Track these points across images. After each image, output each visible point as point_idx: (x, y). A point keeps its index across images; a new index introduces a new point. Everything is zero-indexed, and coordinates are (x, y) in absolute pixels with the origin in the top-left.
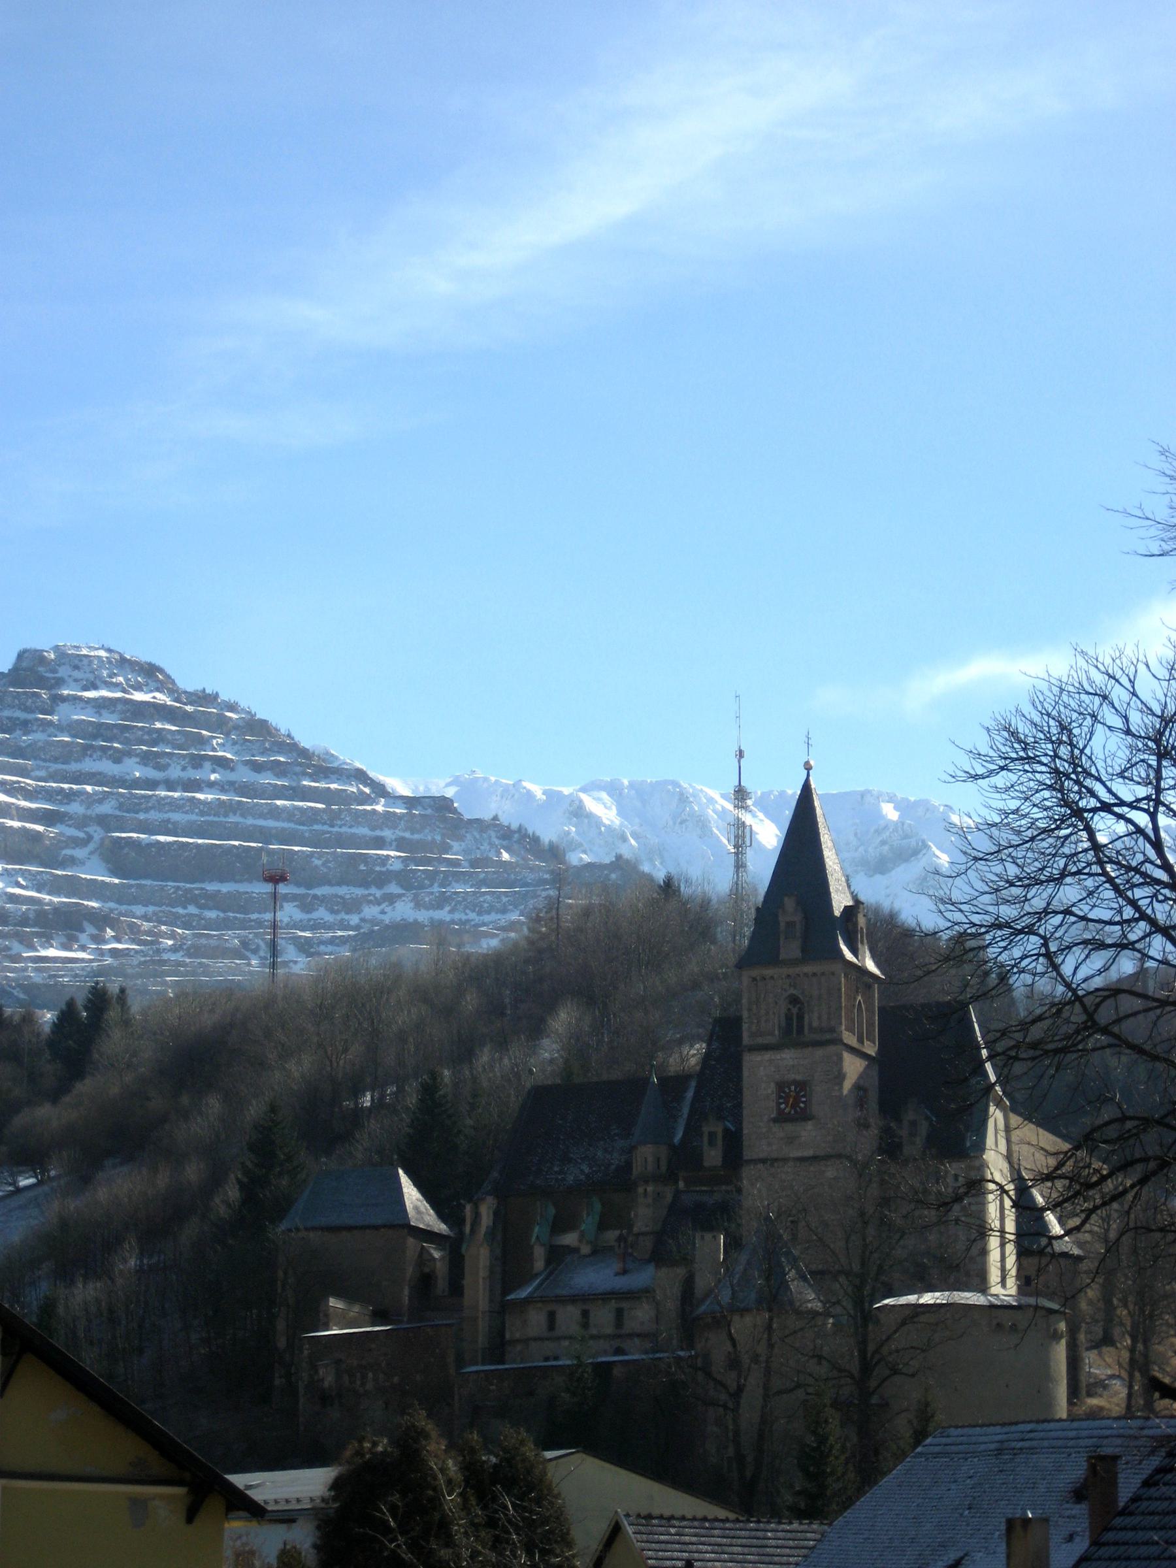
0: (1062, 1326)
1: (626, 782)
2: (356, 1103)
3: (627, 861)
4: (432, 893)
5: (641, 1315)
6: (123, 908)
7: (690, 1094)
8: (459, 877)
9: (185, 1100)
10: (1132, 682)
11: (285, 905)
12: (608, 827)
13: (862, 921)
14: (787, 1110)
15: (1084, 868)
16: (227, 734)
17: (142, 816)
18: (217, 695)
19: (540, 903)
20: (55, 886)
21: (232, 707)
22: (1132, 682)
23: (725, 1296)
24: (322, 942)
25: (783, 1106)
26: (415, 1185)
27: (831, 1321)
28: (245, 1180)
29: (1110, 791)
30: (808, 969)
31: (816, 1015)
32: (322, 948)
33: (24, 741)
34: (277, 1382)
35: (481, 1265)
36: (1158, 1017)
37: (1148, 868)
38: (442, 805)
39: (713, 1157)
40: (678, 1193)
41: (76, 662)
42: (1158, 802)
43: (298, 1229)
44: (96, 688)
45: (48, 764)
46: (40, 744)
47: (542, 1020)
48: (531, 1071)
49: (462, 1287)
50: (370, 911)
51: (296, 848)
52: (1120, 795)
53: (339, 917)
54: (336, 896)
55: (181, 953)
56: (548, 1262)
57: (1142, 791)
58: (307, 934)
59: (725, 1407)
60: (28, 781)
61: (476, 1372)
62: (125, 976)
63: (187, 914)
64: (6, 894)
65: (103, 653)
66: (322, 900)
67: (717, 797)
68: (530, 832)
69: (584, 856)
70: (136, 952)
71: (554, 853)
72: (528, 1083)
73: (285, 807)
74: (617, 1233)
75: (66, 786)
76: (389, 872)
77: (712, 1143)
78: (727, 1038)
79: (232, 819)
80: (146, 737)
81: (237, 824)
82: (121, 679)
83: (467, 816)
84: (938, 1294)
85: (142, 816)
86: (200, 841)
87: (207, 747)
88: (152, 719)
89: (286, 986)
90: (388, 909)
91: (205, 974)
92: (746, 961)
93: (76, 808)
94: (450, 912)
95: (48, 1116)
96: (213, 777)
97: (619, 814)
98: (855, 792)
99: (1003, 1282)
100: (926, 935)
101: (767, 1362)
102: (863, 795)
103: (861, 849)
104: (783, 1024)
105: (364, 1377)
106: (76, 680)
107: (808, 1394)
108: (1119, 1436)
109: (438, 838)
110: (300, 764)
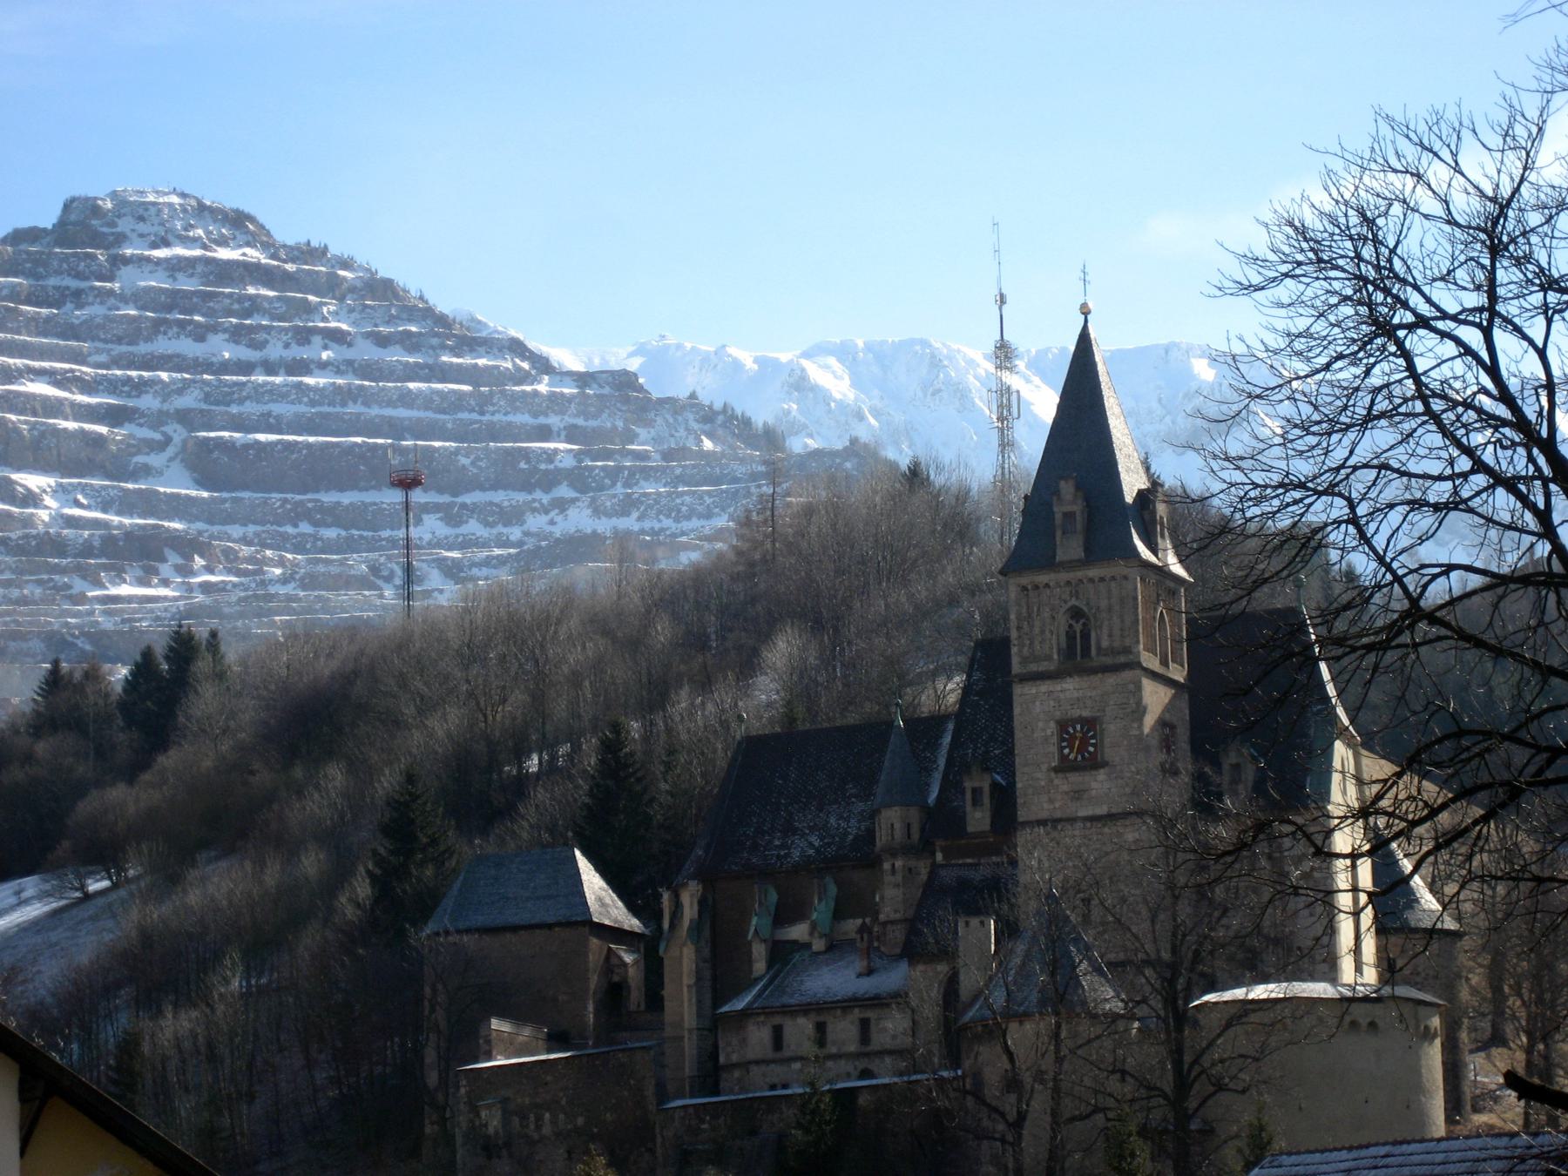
0: (1436, 1022)
1: (860, 344)
2: (520, 768)
3: (866, 445)
4: (615, 496)
5: (892, 1027)
6: (216, 529)
7: (947, 740)
8: (647, 473)
9: (298, 772)
10: (1454, 155)
11: (425, 517)
12: (840, 404)
13: (1161, 509)
14: (1072, 756)
15: (1400, 405)
16: (341, 299)
17: (234, 409)
18: (325, 250)
19: (750, 502)
20: (126, 504)
21: (346, 264)
22: (1454, 155)
23: (998, 998)
24: (474, 565)
25: (1066, 751)
26: (597, 869)
27: (1136, 1024)
28: (378, 871)
29: (1429, 300)
30: (1093, 572)
31: (1105, 631)
32: (475, 571)
33: (78, 317)
34: (428, 1130)
35: (685, 970)
36: (1501, 598)
37: (1483, 400)
38: (624, 382)
39: (979, 819)
40: (935, 867)
41: (141, 211)
42: (1494, 313)
43: (447, 933)
44: (167, 244)
45: (110, 346)
46: (98, 320)
47: (755, 652)
48: (740, 717)
49: (662, 999)
50: (535, 522)
51: (437, 444)
52: (1443, 306)
53: (495, 531)
54: (491, 504)
55: (293, 585)
56: (770, 964)
57: (1474, 300)
58: (455, 554)
59: (1003, 1141)
60: (84, 369)
61: (684, 1107)
62: (221, 616)
63: (299, 535)
64: (62, 516)
65: (175, 200)
66: (473, 510)
67: (979, 359)
68: (739, 412)
69: (809, 441)
70: (235, 585)
71: (771, 439)
72: (739, 732)
73: (420, 392)
74: (859, 921)
75: (134, 373)
76: (557, 470)
78: (991, 665)
79: (352, 409)
80: (236, 306)
81: (360, 414)
82: (200, 232)
83: (656, 394)
84: (1272, 986)
85: (234, 409)
86: (311, 439)
87: (317, 317)
88: (242, 282)
89: (424, 621)
90: (559, 519)
91: (325, 610)
92: (1016, 563)
93: (148, 402)
94: (639, 519)
95: (123, 800)
96: (325, 355)
97: (854, 385)
98: (1156, 346)
99: (1358, 969)
100: (1194, 501)
101: (1055, 1079)
102: (1167, 349)
103: (1168, 419)
104: (1064, 645)
105: (539, 1119)
106: (141, 236)
107: (1108, 1120)
108: (1499, 1158)
109: (620, 424)
110: (437, 335)
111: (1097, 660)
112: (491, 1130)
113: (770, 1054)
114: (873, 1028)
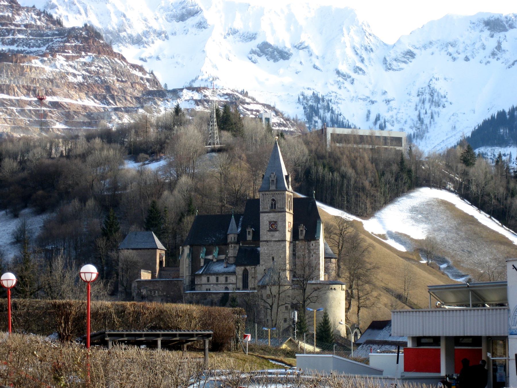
4: (9, 39)
8: (19, 31)
39: (249, 237)
94: (17, 46)
103: (174, 10)
105: (155, 292)
111: (277, 209)
112: (143, 294)
113: (206, 282)
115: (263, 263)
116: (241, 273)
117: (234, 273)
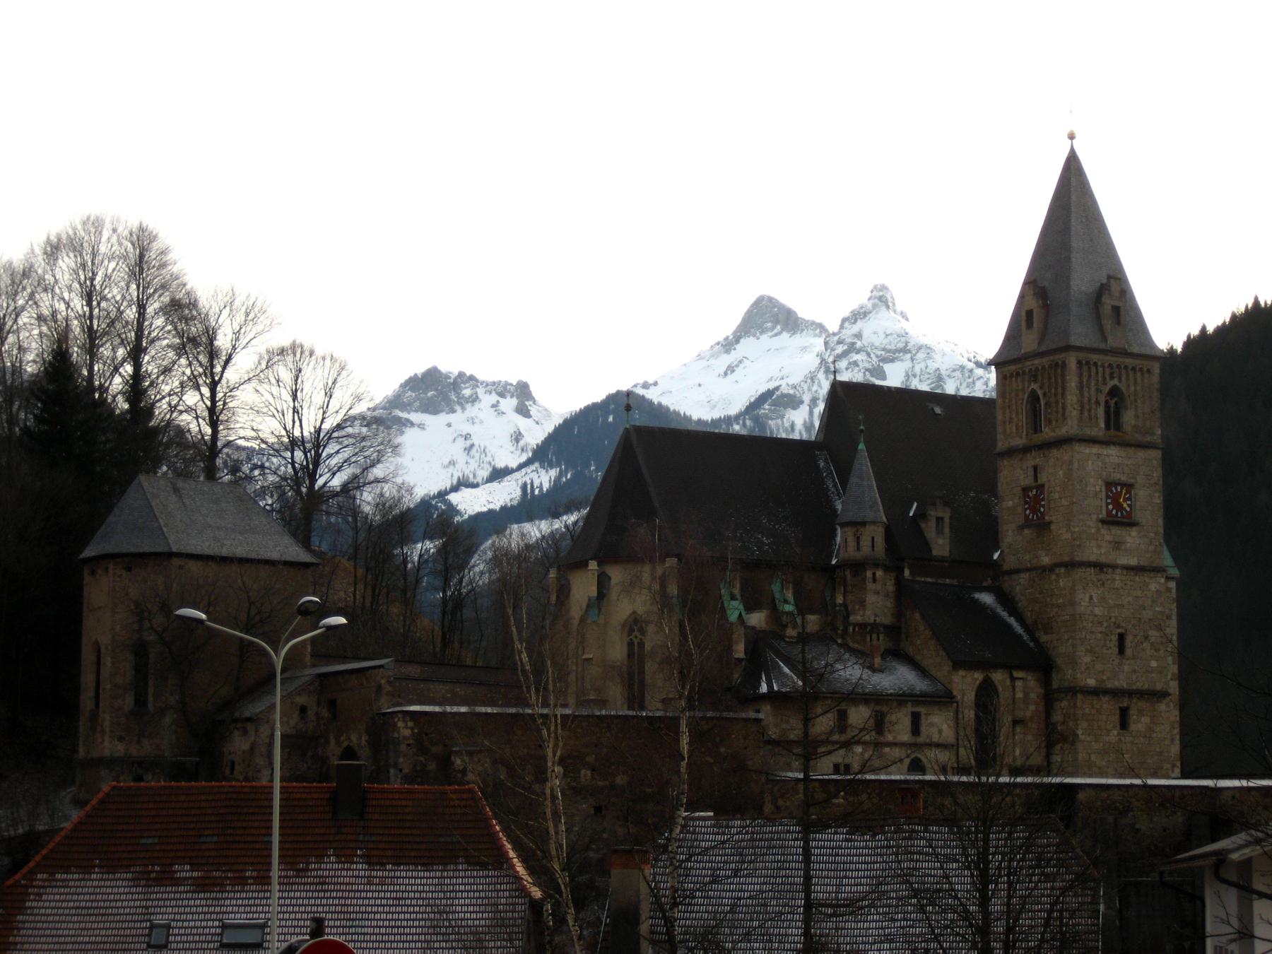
77: (940, 531)
114: (923, 722)
115: (1087, 659)
116: (970, 697)
117: (943, 698)
